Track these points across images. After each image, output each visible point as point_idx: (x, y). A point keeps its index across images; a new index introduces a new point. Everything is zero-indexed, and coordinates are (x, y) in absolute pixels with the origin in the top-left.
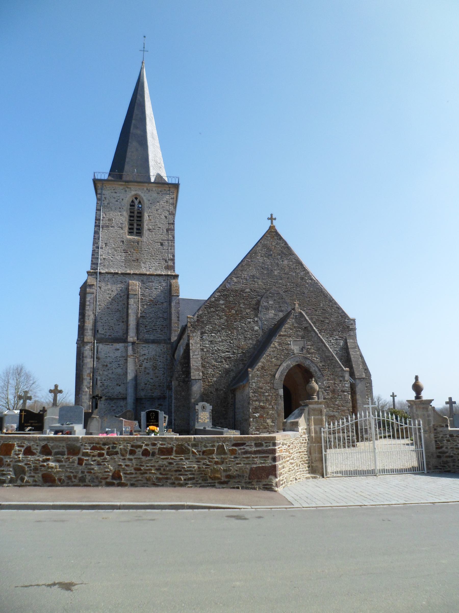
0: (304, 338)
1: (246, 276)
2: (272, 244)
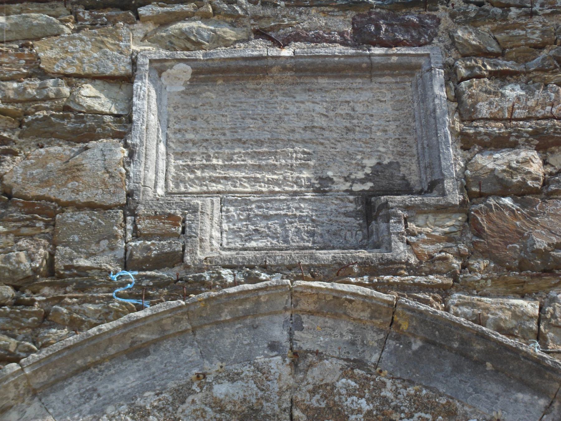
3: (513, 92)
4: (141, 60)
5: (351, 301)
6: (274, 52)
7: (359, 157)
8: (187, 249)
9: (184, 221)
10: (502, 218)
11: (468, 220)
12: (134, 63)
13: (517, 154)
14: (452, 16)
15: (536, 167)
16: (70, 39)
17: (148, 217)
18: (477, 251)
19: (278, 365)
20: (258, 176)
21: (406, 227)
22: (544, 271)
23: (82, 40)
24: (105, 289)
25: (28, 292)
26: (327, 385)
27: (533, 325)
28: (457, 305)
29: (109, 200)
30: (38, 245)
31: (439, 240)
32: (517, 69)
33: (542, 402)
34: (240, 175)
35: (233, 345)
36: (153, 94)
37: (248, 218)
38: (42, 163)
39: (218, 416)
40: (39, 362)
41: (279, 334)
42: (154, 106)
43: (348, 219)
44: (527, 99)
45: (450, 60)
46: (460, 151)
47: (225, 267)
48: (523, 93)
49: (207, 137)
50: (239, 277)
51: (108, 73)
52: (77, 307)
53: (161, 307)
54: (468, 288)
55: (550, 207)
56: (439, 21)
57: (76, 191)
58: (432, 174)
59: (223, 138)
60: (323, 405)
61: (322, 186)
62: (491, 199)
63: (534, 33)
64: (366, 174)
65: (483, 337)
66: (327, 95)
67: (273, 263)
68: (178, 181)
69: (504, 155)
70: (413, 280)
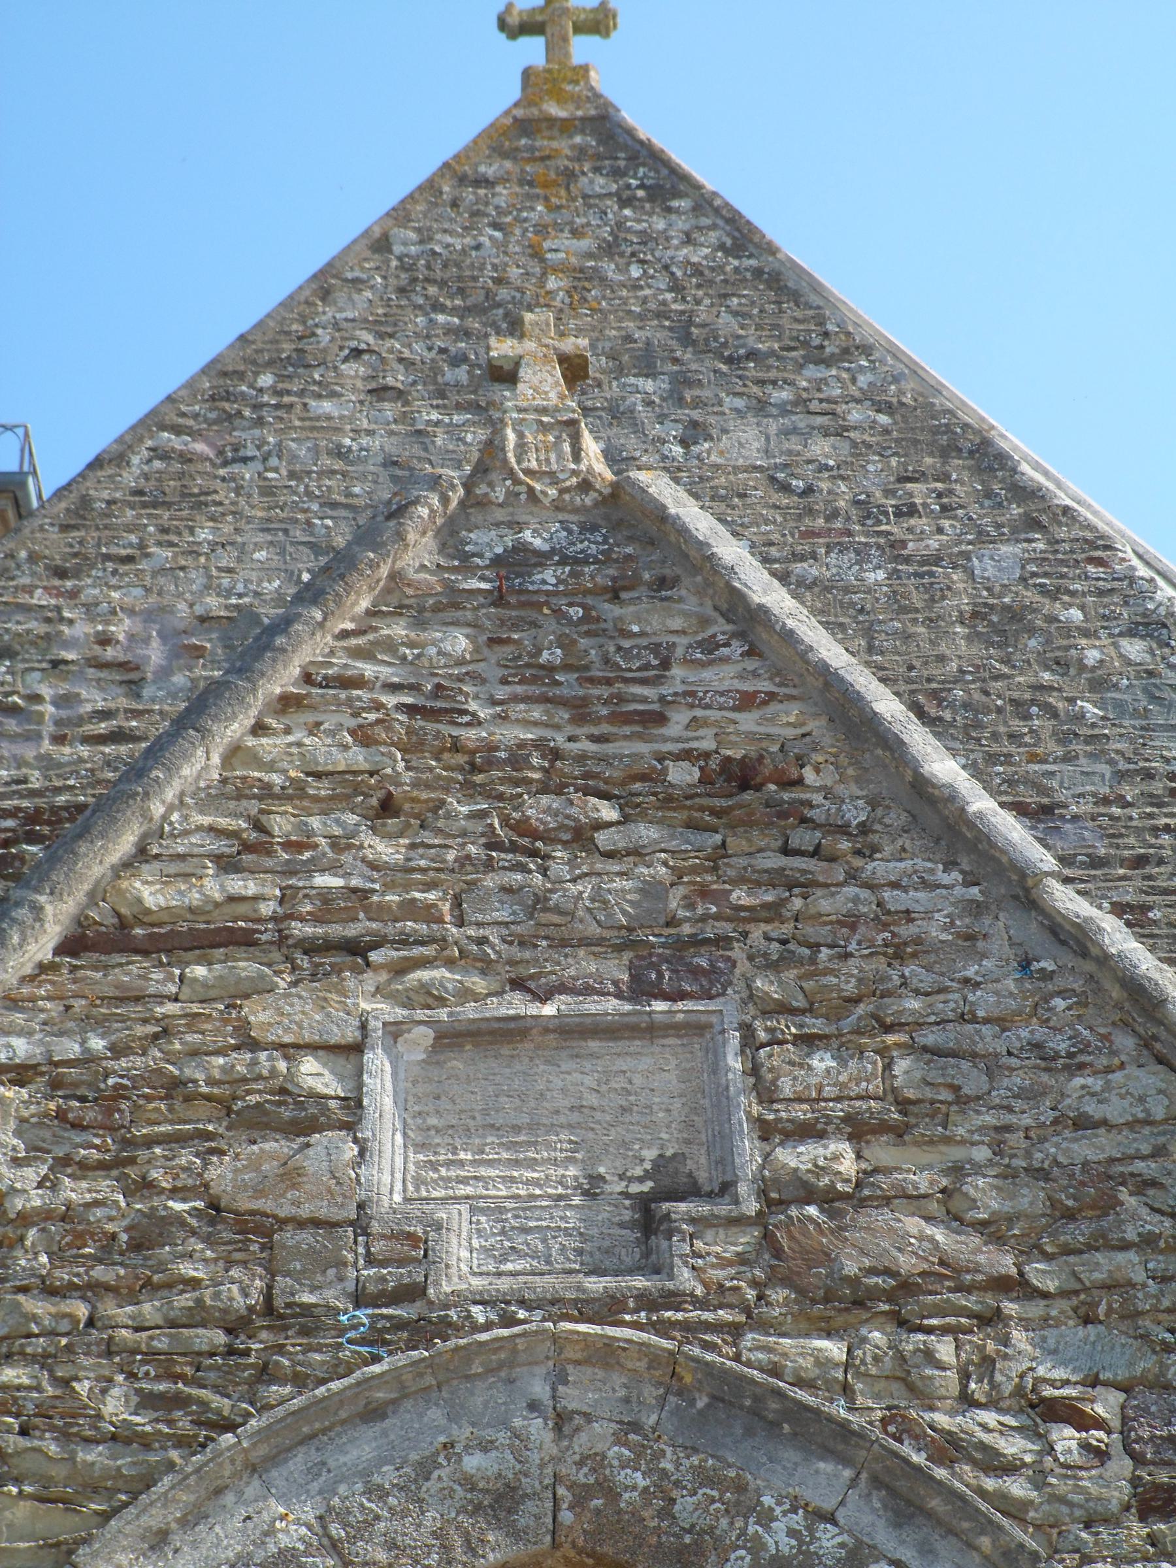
0: (711, 983)
1: (120, 629)
2: (536, 254)
3: (822, 1062)
4: (372, 1024)
5: (624, 1349)
6: (534, 1009)
7: (637, 1147)
8: (431, 1279)
9: (426, 1242)
10: (805, 1233)
11: (765, 1236)
12: (363, 1027)
13: (825, 1147)
14: (751, 958)
15: (848, 1165)
16: (287, 996)
17: (384, 1237)
18: (775, 1278)
19: (538, 1429)
20: (515, 1174)
21: (692, 1245)
22: (854, 1303)
23: (300, 997)
24: (333, 1332)
25: (243, 1337)
26: (596, 1454)
27: (840, 1375)
28: (750, 1350)
29: (337, 1215)
30: (253, 1275)
31: (730, 1263)
32: (827, 1031)
33: (848, 1473)
34: (493, 1173)
35: (486, 1404)
36: (388, 1068)
37: (503, 1232)
38: (254, 1164)
39: (469, 1496)
40: (259, 1432)
41: (540, 1389)
42: (389, 1085)
43: (624, 1232)
44: (839, 1073)
45: (747, 1018)
46: (757, 1143)
47: (475, 1303)
48: (834, 1064)
49: (454, 1122)
50: (494, 1317)
51: (333, 1042)
52: (300, 1357)
53: (401, 1359)
54: (765, 1326)
55: (862, 1220)
56: (734, 965)
57: (296, 1203)
58: (724, 1172)
59: (471, 1123)
60: (592, 1480)
61: (592, 1188)
62: (793, 1208)
63: (848, 982)
64: (646, 1171)
65: (779, 1393)
66: (599, 1062)
67: (533, 1297)
68: (419, 1182)
69: (810, 1147)
70: (699, 1317)
